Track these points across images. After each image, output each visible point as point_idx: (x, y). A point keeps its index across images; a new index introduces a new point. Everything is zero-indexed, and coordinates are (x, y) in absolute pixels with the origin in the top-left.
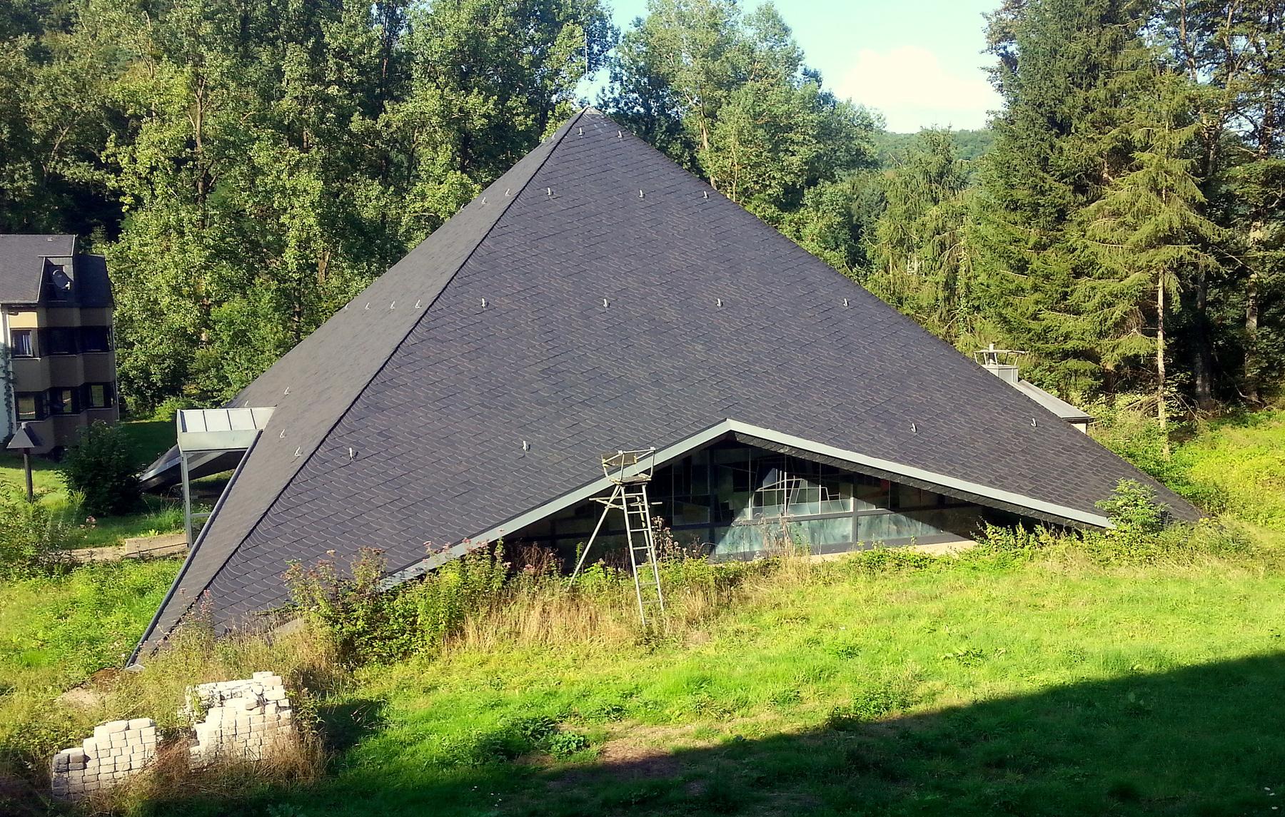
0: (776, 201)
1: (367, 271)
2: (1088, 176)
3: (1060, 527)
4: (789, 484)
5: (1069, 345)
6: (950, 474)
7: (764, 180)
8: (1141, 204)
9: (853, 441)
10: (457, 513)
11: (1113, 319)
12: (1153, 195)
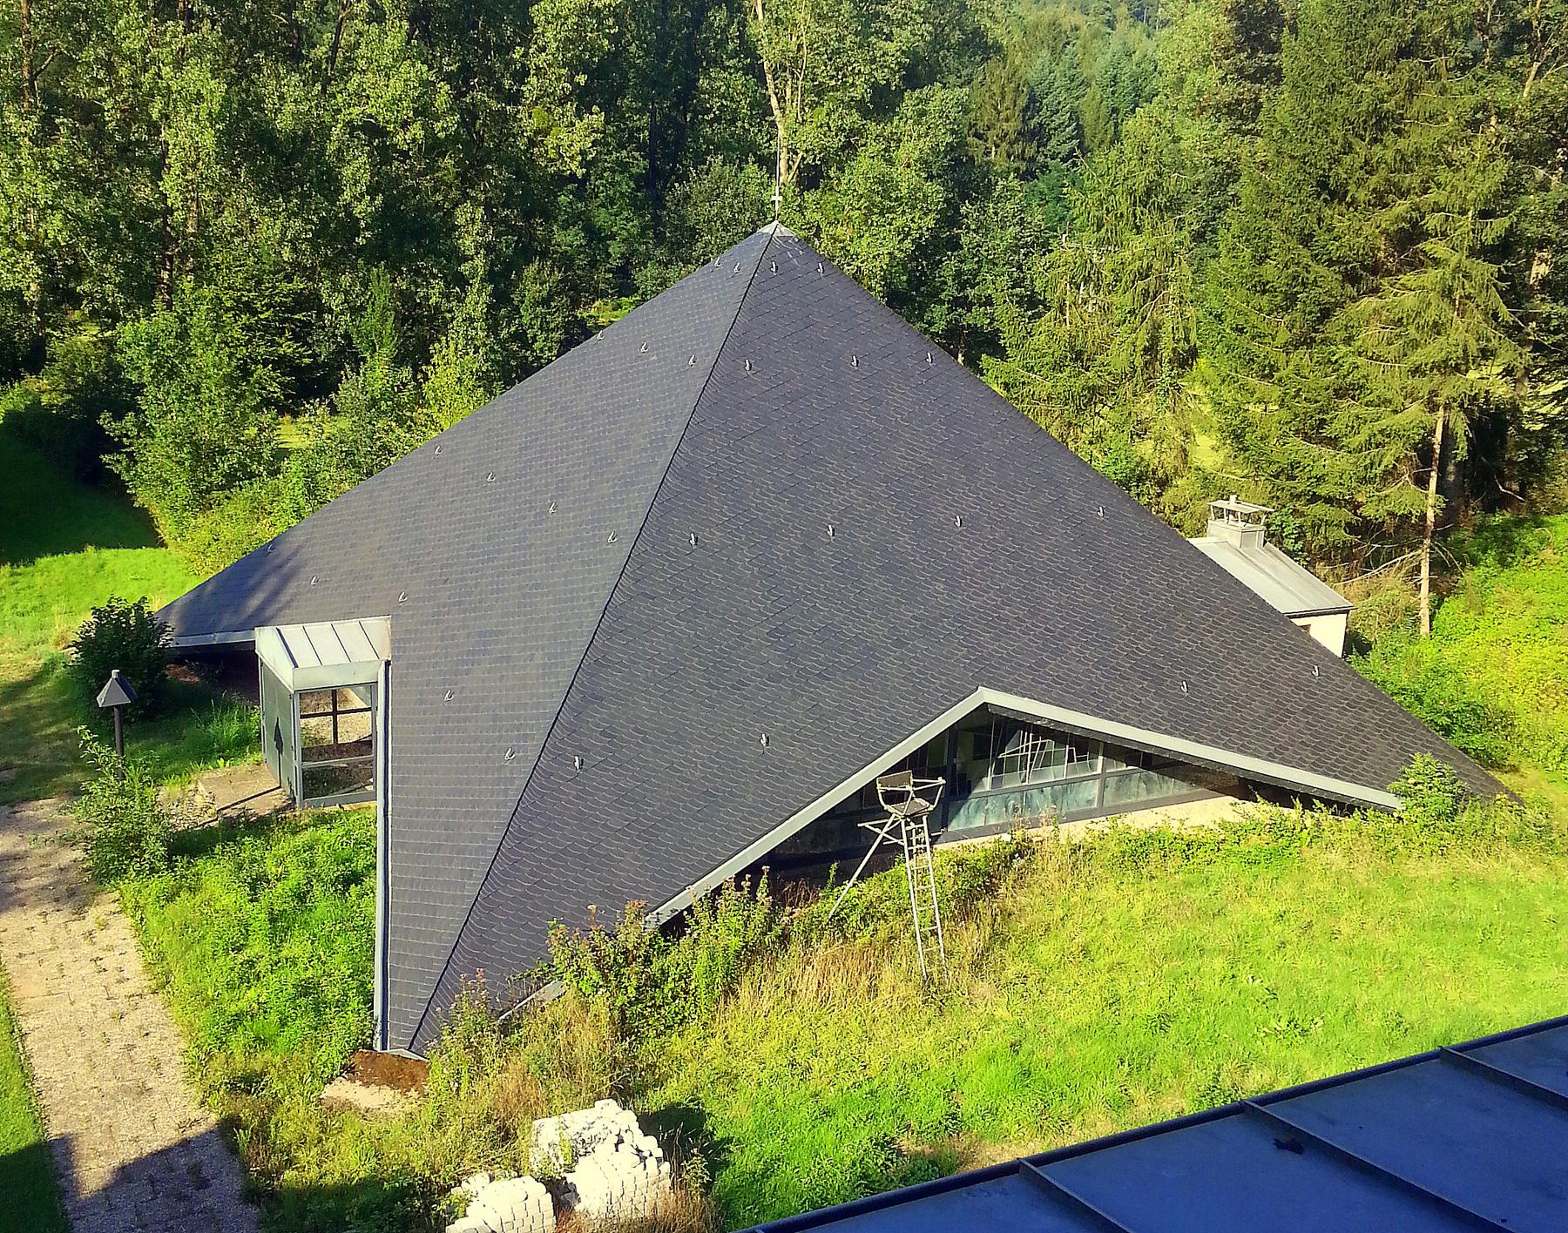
0: (860, 105)
1: (283, 211)
2: (1364, 268)
3: (1344, 807)
4: (1034, 749)
5: (1323, 490)
6: (1226, 747)
7: (845, 76)
8: (1431, 315)
9: (1117, 708)
10: (700, 834)
11: (1382, 467)
12: (1445, 305)
